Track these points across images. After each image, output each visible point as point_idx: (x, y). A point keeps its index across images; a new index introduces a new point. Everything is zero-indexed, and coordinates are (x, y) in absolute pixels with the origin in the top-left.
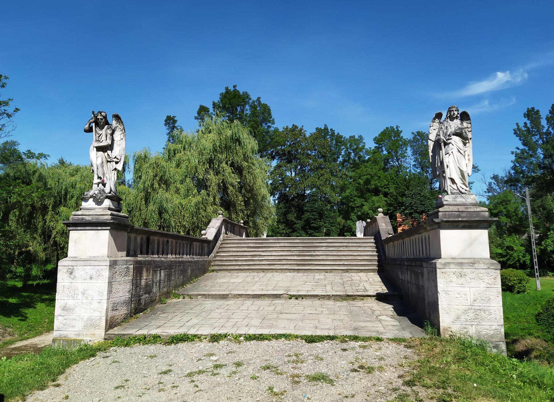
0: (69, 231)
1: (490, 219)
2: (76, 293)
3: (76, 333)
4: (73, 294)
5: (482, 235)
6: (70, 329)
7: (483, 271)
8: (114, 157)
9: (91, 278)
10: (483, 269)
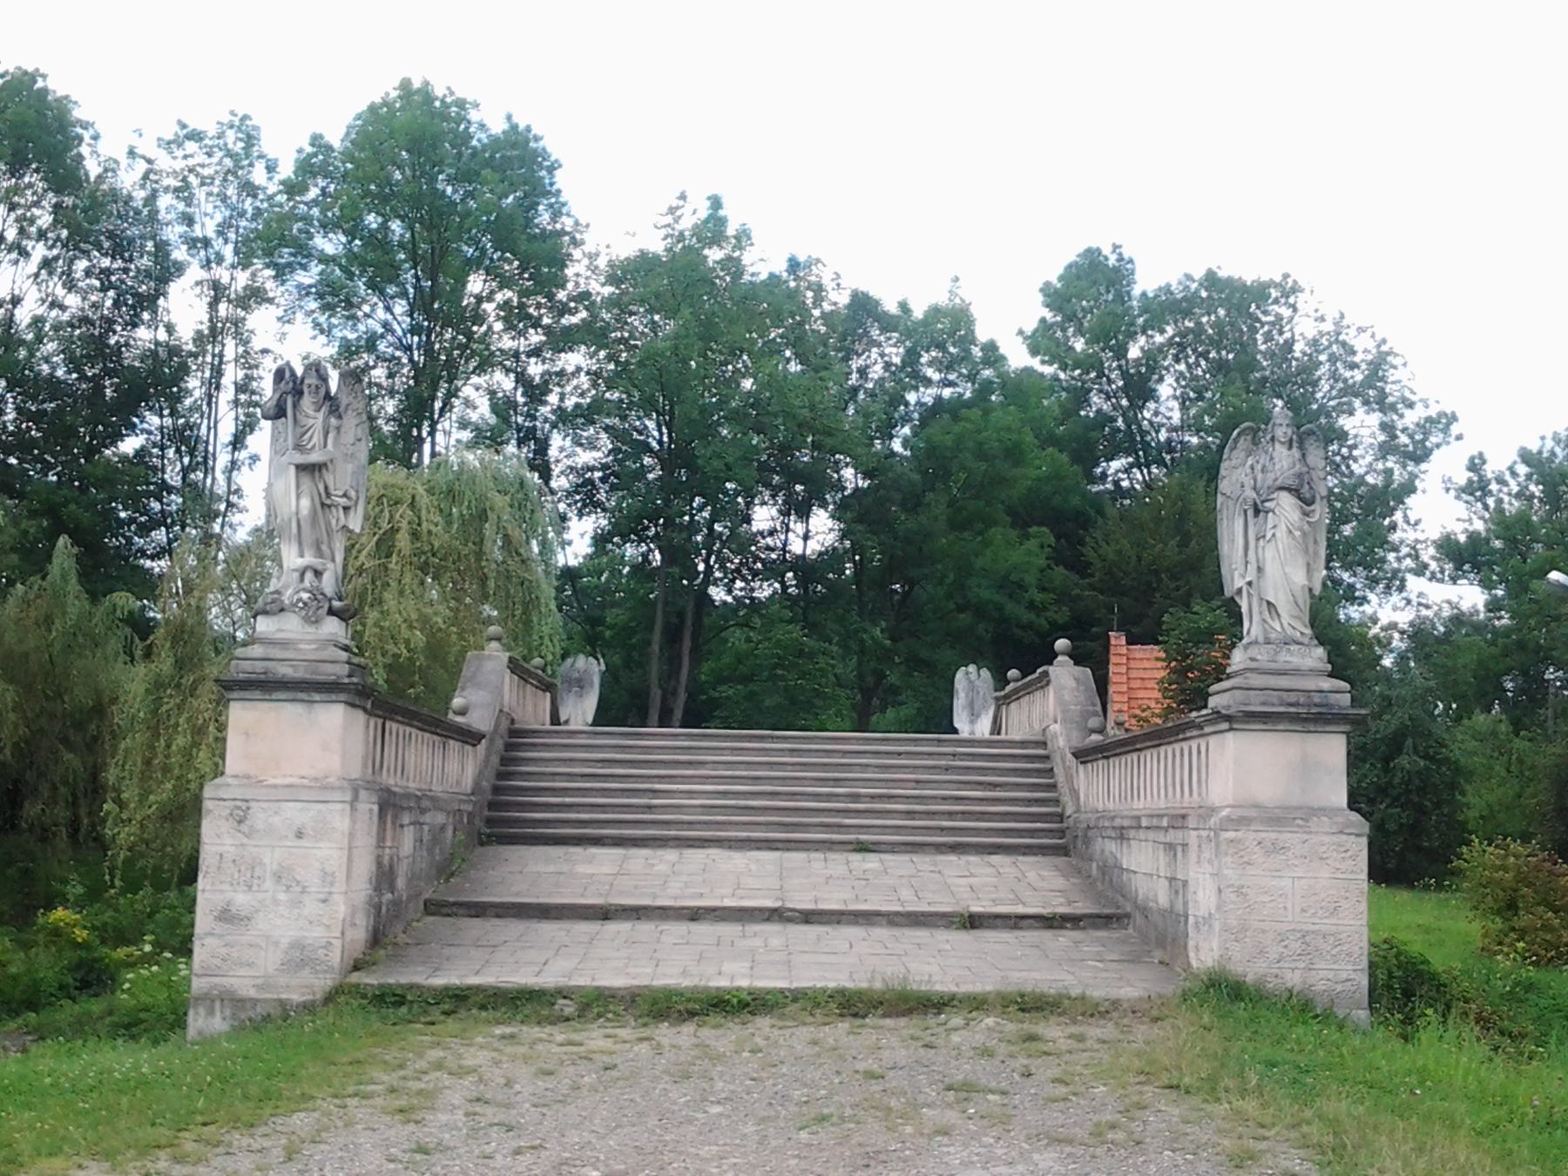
0: (222, 703)
1: (1351, 711)
2: (256, 875)
3: (259, 981)
4: (249, 876)
5: (1332, 750)
6: (242, 972)
7: (1327, 839)
8: (341, 493)
9: (299, 835)
10: (1327, 833)
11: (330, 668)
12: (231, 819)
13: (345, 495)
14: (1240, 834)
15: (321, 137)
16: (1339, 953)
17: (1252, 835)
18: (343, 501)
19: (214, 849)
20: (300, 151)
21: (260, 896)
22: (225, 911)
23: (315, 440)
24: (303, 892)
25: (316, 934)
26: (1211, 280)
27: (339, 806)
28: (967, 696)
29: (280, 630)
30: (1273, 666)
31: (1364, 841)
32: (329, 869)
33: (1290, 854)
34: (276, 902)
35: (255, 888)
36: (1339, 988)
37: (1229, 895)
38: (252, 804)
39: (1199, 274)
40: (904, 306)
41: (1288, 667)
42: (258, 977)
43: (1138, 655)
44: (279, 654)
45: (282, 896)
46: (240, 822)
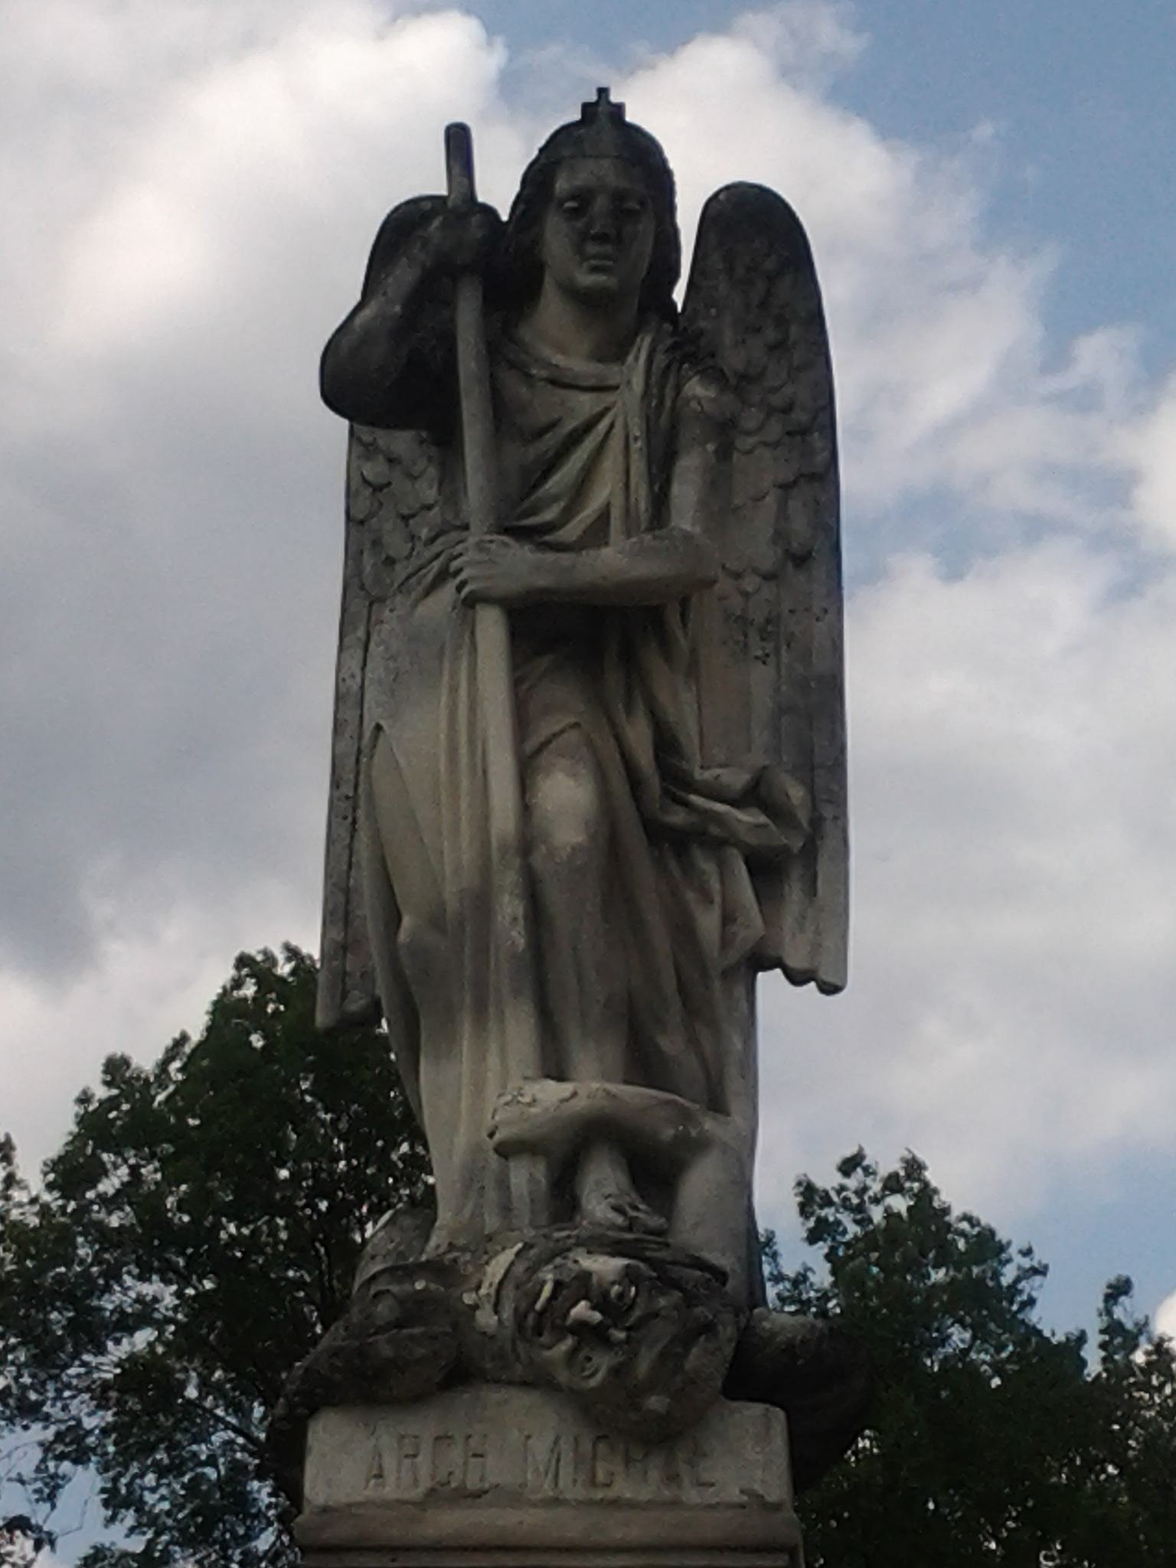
8: (736, 779)
13: (755, 795)
15: (125, 1062)
20: (84, 1099)
23: (604, 491)
29: (439, 1495)
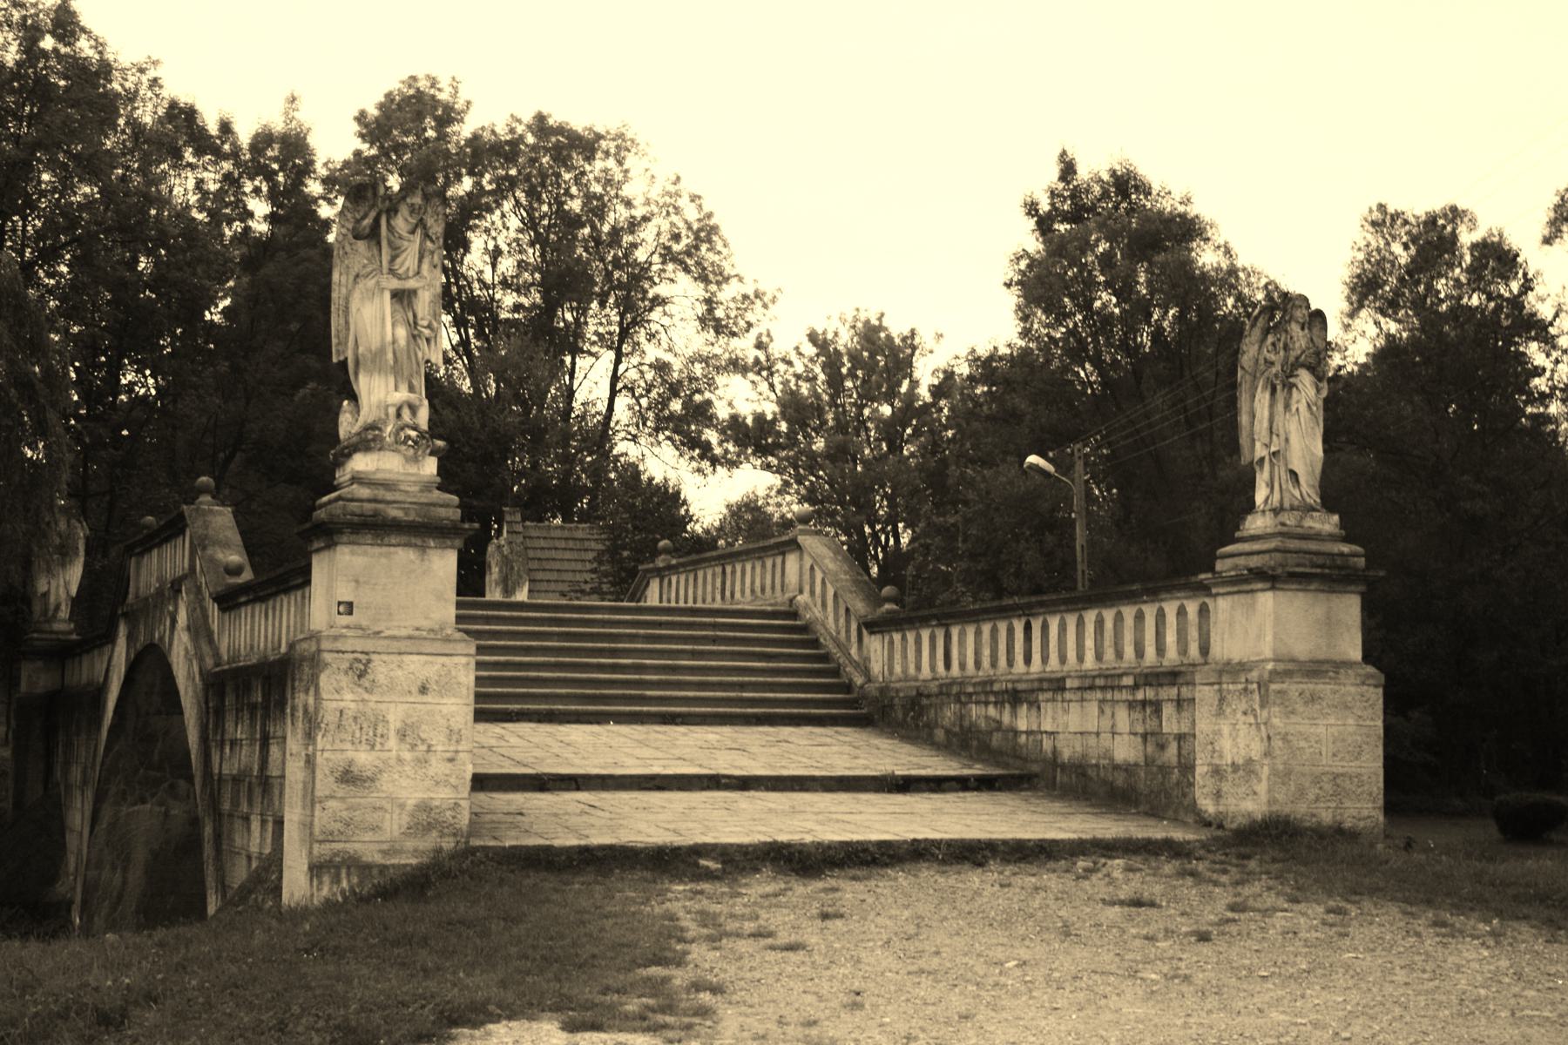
2: (379, 731)
3: (385, 847)
4: (371, 734)
5: (1349, 608)
9: (423, 690)
11: (442, 512)
12: (350, 673)
14: (1284, 686)
16: (1362, 793)
17: (1294, 687)
18: (427, 332)
19: (334, 705)
21: (385, 755)
22: (347, 772)
24: (428, 751)
25: (442, 796)
26: (541, 125)
27: (464, 660)
28: (501, 571)
30: (1299, 530)
31: (1380, 690)
32: (455, 727)
33: (1324, 704)
34: (400, 760)
35: (378, 747)
36: (1362, 824)
37: (1277, 743)
38: (374, 657)
39: (527, 117)
40: (226, 128)
41: (1312, 532)
42: (382, 842)
43: (534, 533)
44: (389, 496)
45: (407, 756)
46: (360, 676)
